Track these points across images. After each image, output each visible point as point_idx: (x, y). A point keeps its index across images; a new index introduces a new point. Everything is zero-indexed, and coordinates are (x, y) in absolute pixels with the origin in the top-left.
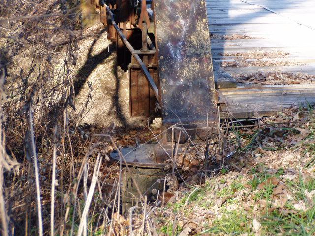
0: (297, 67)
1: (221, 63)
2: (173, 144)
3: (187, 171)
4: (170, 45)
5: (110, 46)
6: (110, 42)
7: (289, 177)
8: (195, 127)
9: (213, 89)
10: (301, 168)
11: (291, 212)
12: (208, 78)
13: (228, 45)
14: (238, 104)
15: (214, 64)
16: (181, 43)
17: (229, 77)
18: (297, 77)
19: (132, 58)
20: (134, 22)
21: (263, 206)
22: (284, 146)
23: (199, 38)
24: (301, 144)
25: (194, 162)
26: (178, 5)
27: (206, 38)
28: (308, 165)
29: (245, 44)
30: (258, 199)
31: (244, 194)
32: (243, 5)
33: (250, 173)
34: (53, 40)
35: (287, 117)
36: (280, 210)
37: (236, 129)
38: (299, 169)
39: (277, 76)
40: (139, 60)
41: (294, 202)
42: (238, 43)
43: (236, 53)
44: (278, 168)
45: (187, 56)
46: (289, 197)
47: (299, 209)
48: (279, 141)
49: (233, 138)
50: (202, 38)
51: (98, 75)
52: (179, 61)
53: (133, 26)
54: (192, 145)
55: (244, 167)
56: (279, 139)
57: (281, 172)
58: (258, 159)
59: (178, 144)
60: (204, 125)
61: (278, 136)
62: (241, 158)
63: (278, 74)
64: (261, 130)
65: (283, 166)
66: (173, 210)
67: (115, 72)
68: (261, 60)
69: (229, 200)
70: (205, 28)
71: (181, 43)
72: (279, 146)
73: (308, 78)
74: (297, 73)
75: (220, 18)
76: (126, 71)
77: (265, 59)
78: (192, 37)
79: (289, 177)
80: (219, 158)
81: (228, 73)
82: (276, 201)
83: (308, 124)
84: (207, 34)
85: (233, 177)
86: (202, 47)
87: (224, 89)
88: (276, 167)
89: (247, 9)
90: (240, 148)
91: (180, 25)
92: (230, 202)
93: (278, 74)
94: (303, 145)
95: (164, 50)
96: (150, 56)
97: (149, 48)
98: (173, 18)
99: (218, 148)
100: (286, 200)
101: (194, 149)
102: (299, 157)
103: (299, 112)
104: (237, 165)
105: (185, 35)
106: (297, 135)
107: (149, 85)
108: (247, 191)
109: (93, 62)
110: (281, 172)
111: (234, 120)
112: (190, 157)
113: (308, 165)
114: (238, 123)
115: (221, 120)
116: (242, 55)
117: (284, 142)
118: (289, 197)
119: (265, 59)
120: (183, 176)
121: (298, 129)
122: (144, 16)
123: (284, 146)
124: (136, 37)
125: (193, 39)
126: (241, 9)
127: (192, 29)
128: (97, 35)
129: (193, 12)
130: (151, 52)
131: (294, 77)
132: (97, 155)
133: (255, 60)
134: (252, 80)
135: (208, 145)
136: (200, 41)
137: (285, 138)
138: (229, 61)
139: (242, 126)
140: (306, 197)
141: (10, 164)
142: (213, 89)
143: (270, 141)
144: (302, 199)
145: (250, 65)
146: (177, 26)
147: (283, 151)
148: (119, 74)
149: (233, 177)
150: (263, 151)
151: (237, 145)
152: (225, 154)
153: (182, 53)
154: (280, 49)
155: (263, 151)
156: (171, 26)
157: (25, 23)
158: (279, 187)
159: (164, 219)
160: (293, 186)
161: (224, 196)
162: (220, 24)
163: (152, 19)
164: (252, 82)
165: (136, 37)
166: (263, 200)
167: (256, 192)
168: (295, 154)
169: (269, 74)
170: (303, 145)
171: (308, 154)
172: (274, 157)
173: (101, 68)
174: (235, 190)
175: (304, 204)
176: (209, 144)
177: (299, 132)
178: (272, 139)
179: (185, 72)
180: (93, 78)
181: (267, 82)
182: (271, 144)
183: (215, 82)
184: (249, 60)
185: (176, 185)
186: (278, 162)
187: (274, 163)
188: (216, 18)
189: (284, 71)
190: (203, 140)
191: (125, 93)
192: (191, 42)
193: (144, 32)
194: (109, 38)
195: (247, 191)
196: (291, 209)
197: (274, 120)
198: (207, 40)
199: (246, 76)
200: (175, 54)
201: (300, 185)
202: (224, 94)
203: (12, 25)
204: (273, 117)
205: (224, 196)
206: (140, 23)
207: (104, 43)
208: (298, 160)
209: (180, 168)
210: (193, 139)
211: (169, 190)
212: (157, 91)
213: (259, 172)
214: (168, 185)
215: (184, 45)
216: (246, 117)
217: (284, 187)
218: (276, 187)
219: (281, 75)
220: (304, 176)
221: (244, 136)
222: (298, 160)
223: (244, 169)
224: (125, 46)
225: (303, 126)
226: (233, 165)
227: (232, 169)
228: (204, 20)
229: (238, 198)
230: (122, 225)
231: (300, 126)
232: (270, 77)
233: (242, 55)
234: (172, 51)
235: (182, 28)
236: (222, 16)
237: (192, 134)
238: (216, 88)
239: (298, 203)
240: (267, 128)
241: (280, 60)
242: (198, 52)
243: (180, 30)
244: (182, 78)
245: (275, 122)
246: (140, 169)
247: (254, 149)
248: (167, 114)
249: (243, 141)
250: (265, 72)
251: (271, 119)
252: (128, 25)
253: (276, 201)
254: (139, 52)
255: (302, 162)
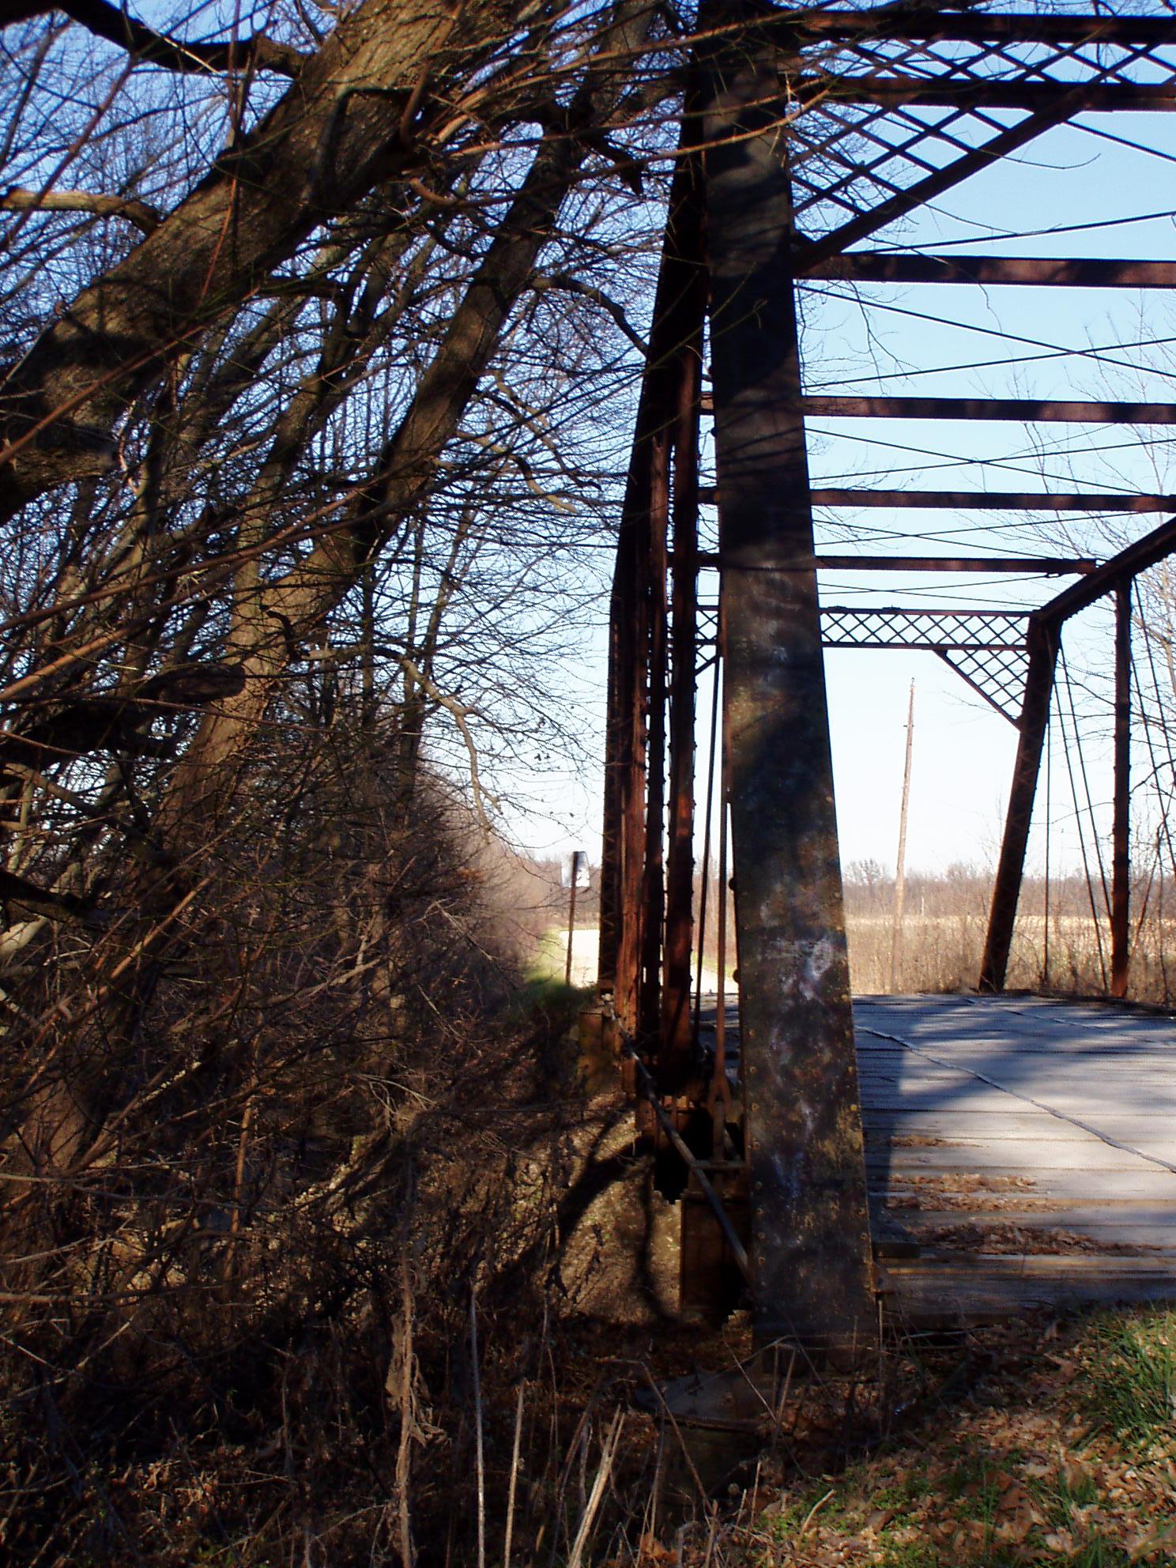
0: (1050, 1216)
1: (885, 1200)
2: (776, 1379)
3: (803, 1441)
4: (777, 1159)
5: (638, 1140)
6: (639, 1134)
7: (1034, 1469)
8: (824, 1342)
9: (868, 1261)
10: (1062, 1451)
11: (1042, 1553)
12: (858, 1235)
13: (897, 1159)
14: (921, 1295)
15: (872, 1201)
16: (801, 1155)
17: (903, 1234)
18: (1053, 1239)
19: (691, 1176)
20: (695, 1096)
21: (975, 1534)
22: (1023, 1397)
23: (842, 1147)
24: (1062, 1395)
25: (820, 1421)
26: (797, 1072)
27: (857, 1147)
28: (1078, 1444)
29: (935, 1158)
30: (965, 1519)
31: (934, 1504)
32: (933, 1068)
33: (946, 1456)
34: (521, 1120)
35: (1030, 1330)
36: (1015, 1549)
37: (917, 1352)
38: (1057, 1453)
39: (1010, 1235)
40: (706, 1183)
41: (1047, 1529)
42: (923, 1155)
43: (917, 1179)
44: (1011, 1447)
45: (813, 1185)
46: (1036, 1517)
47: (1059, 1547)
48: (1011, 1384)
49: (910, 1372)
50: (847, 1147)
51: (609, 1203)
52: (795, 1195)
53: (692, 1105)
54: (816, 1383)
55: (932, 1439)
56: (1011, 1379)
57: (1015, 1456)
58: (965, 1422)
59: (787, 1380)
60: (849, 1341)
61: (1010, 1373)
62: (927, 1418)
63: (1012, 1230)
64: (973, 1358)
65: (1020, 1443)
66: (773, 1534)
67: (645, 1198)
68: (973, 1195)
69: (899, 1517)
70: (854, 1125)
71: (801, 1155)
72: (1011, 1395)
73: (1077, 1243)
74: (1054, 1230)
75: (882, 1096)
76: (673, 1203)
77: (982, 1195)
78: (827, 1143)
79: (1034, 1469)
80: (876, 1413)
81: (897, 1223)
82: (1006, 1525)
83: (1076, 1350)
84: (858, 1137)
85: (907, 1461)
86: (847, 1165)
87: (891, 1261)
88: (1006, 1443)
89: (942, 1079)
90: (924, 1395)
91: (801, 1116)
92: (901, 1522)
93: (1012, 1230)
94: (1068, 1395)
95: (764, 1168)
96: (728, 1175)
97: (728, 1156)
98: (789, 1103)
99: (874, 1394)
100: (1027, 1524)
101: (822, 1392)
102: (1057, 1424)
103: (1059, 1320)
104: (917, 1435)
105: (811, 1139)
106: (1053, 1373)
107: (725, 1238)
108: (939, 1499)
109: (599, 1175)
110: (1015, 1456)
111: (912, 1332)
112: (812, 1409)
113: (1078, 1444)
114: (921, 1339)
115: (886, 1330)
116: (931, 1181)
117: (1023, 1388)
118: (1036, 1517)
119: (982, 1195)
120: (794, 1450)
121: (1056, 1359)
122: (717, 1085)
123: (1023, 1397)
124: (698, 1128)
125: (828, 1147)
126: (929, 1078)
127: (826, 1125)
128: (609, 1121)
129: (829, 1089)
130: (733, 1165)
131: (1046, 1238)
132: (599, 1366)
133: (960, 1197)
134: (953, 1241)
135: (854, 1385)
136: (843, 1152)
137: (1025, 1378)
138: (902, 1195)
139: (931, 1347)
140: (1073, 1519)
141: (426, 1433)
142: (868, 1261)
143: (992, 1383)
144: (1063, 1524)
145: (949, 1207)
146: (794, 1118)
147: (1022, 1408)
148: (656, 1203)
149: (907, 1461)
150: (977, 1406)
151: (918, 1387)
152: (891, 1408)
153: (803, 1176)
154: (1014, 1173)
155: (977, 1406)
156: (781, 1117)
157: (460, 1083)
158: (1014, 1493)
159: (754, 1553)
160: (1043, 1491)
161: (889, 1506)
162: (884, 1110)
163: (735, 1091)
164: (951, 1247)
165: (698, 1128)
166: (977, 1523)
167: (960, 1501)
168: (1049, 1417)
169: (992, 1229)
170: (1068, 1395)
171: (1077, 1418)
172: (1000, 1421)
173: (616, 1189)
174: (912, 1494)
175: (1069, 1536)
176: (856, 1383)
177: (1057, 1367)
178: (996, 1379)
179: (807, 1218)
180: (596, 1212)
181: (986, 1248)
182: (994, 1390)
183: (874, 1244)
184: (948, 1195)
185: (780, 1476)
186: (1009, 1434)
187: (1001, 1434)
188: (876, 1096)
189: (1022, 1223)
190: (841, 1372)
191: (668, 1250)
192: (824, 1154)
193: (718, 1122)
194: (638, 1125)
195: (939, 1499)
196: (1040, 1547)
197: (1002, 1336)
198: (859, 1152)
199: (939, 1230)
200: (789, 1180)
201: (1060, 1489)
202: (891, 1271)
203: (430, 1086)
204: (1000, 1328)
205: (889, 1506)
206: (711, 1099)
207: (625, 1134)
208: (1054, 1431)
209: (788, 1434)
210: (821, 1369)
211: (766, 1488)
212: (743, 1257)
213: (966, 1453)
214: (764, 1473)
215: (807, 1159)
216: (939, 1326)
217: (1023, 1494)
218: (1005, 1493)
219: (1017, 1233)
220: (1068, 1469)
221: (934, 1369)
222: (1054, 1431)
223: (932, 1445)
224: (672, 1147)
225: (1067, 1354)
226: (910, 1434)
227: (909, 1444)
228: (854, 1107)
229: (920, 1514)
230: (659, 1561)
231: (1059, 1354)
232: (993, 1237)
233: (931, 1181)
234: (781, 1173)
235: (804, 1123)
236: (882, 1091)
237: (816, 1360)
238: (875, 1257)
239: (1055, 1533)
240: (986, 1352)
241: (1015, 1197)
242: (838, 1177)
243: (801, 1126)
244: (801, 1233)
245: (1003, 1341)
246: (700, 1431)
247: (956, 1401)
248: (765, 1310)
249: (933, 1380)
250: (983, 1224)
251: (994, 1334)
252: (682, 1102)
253: (1006, 1525)
254: (705, 1164)
255: (1063, 1438)
